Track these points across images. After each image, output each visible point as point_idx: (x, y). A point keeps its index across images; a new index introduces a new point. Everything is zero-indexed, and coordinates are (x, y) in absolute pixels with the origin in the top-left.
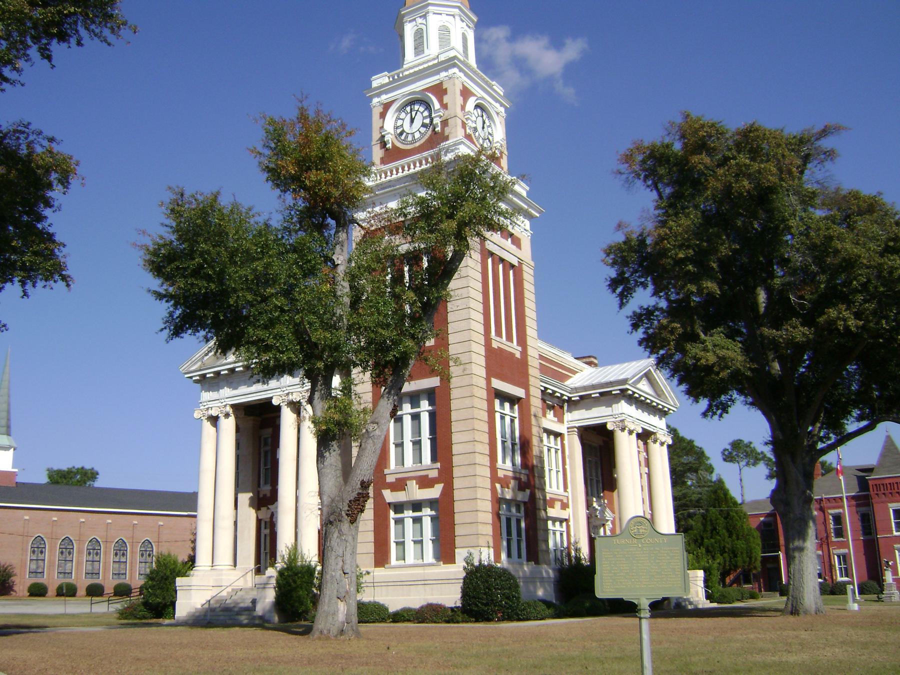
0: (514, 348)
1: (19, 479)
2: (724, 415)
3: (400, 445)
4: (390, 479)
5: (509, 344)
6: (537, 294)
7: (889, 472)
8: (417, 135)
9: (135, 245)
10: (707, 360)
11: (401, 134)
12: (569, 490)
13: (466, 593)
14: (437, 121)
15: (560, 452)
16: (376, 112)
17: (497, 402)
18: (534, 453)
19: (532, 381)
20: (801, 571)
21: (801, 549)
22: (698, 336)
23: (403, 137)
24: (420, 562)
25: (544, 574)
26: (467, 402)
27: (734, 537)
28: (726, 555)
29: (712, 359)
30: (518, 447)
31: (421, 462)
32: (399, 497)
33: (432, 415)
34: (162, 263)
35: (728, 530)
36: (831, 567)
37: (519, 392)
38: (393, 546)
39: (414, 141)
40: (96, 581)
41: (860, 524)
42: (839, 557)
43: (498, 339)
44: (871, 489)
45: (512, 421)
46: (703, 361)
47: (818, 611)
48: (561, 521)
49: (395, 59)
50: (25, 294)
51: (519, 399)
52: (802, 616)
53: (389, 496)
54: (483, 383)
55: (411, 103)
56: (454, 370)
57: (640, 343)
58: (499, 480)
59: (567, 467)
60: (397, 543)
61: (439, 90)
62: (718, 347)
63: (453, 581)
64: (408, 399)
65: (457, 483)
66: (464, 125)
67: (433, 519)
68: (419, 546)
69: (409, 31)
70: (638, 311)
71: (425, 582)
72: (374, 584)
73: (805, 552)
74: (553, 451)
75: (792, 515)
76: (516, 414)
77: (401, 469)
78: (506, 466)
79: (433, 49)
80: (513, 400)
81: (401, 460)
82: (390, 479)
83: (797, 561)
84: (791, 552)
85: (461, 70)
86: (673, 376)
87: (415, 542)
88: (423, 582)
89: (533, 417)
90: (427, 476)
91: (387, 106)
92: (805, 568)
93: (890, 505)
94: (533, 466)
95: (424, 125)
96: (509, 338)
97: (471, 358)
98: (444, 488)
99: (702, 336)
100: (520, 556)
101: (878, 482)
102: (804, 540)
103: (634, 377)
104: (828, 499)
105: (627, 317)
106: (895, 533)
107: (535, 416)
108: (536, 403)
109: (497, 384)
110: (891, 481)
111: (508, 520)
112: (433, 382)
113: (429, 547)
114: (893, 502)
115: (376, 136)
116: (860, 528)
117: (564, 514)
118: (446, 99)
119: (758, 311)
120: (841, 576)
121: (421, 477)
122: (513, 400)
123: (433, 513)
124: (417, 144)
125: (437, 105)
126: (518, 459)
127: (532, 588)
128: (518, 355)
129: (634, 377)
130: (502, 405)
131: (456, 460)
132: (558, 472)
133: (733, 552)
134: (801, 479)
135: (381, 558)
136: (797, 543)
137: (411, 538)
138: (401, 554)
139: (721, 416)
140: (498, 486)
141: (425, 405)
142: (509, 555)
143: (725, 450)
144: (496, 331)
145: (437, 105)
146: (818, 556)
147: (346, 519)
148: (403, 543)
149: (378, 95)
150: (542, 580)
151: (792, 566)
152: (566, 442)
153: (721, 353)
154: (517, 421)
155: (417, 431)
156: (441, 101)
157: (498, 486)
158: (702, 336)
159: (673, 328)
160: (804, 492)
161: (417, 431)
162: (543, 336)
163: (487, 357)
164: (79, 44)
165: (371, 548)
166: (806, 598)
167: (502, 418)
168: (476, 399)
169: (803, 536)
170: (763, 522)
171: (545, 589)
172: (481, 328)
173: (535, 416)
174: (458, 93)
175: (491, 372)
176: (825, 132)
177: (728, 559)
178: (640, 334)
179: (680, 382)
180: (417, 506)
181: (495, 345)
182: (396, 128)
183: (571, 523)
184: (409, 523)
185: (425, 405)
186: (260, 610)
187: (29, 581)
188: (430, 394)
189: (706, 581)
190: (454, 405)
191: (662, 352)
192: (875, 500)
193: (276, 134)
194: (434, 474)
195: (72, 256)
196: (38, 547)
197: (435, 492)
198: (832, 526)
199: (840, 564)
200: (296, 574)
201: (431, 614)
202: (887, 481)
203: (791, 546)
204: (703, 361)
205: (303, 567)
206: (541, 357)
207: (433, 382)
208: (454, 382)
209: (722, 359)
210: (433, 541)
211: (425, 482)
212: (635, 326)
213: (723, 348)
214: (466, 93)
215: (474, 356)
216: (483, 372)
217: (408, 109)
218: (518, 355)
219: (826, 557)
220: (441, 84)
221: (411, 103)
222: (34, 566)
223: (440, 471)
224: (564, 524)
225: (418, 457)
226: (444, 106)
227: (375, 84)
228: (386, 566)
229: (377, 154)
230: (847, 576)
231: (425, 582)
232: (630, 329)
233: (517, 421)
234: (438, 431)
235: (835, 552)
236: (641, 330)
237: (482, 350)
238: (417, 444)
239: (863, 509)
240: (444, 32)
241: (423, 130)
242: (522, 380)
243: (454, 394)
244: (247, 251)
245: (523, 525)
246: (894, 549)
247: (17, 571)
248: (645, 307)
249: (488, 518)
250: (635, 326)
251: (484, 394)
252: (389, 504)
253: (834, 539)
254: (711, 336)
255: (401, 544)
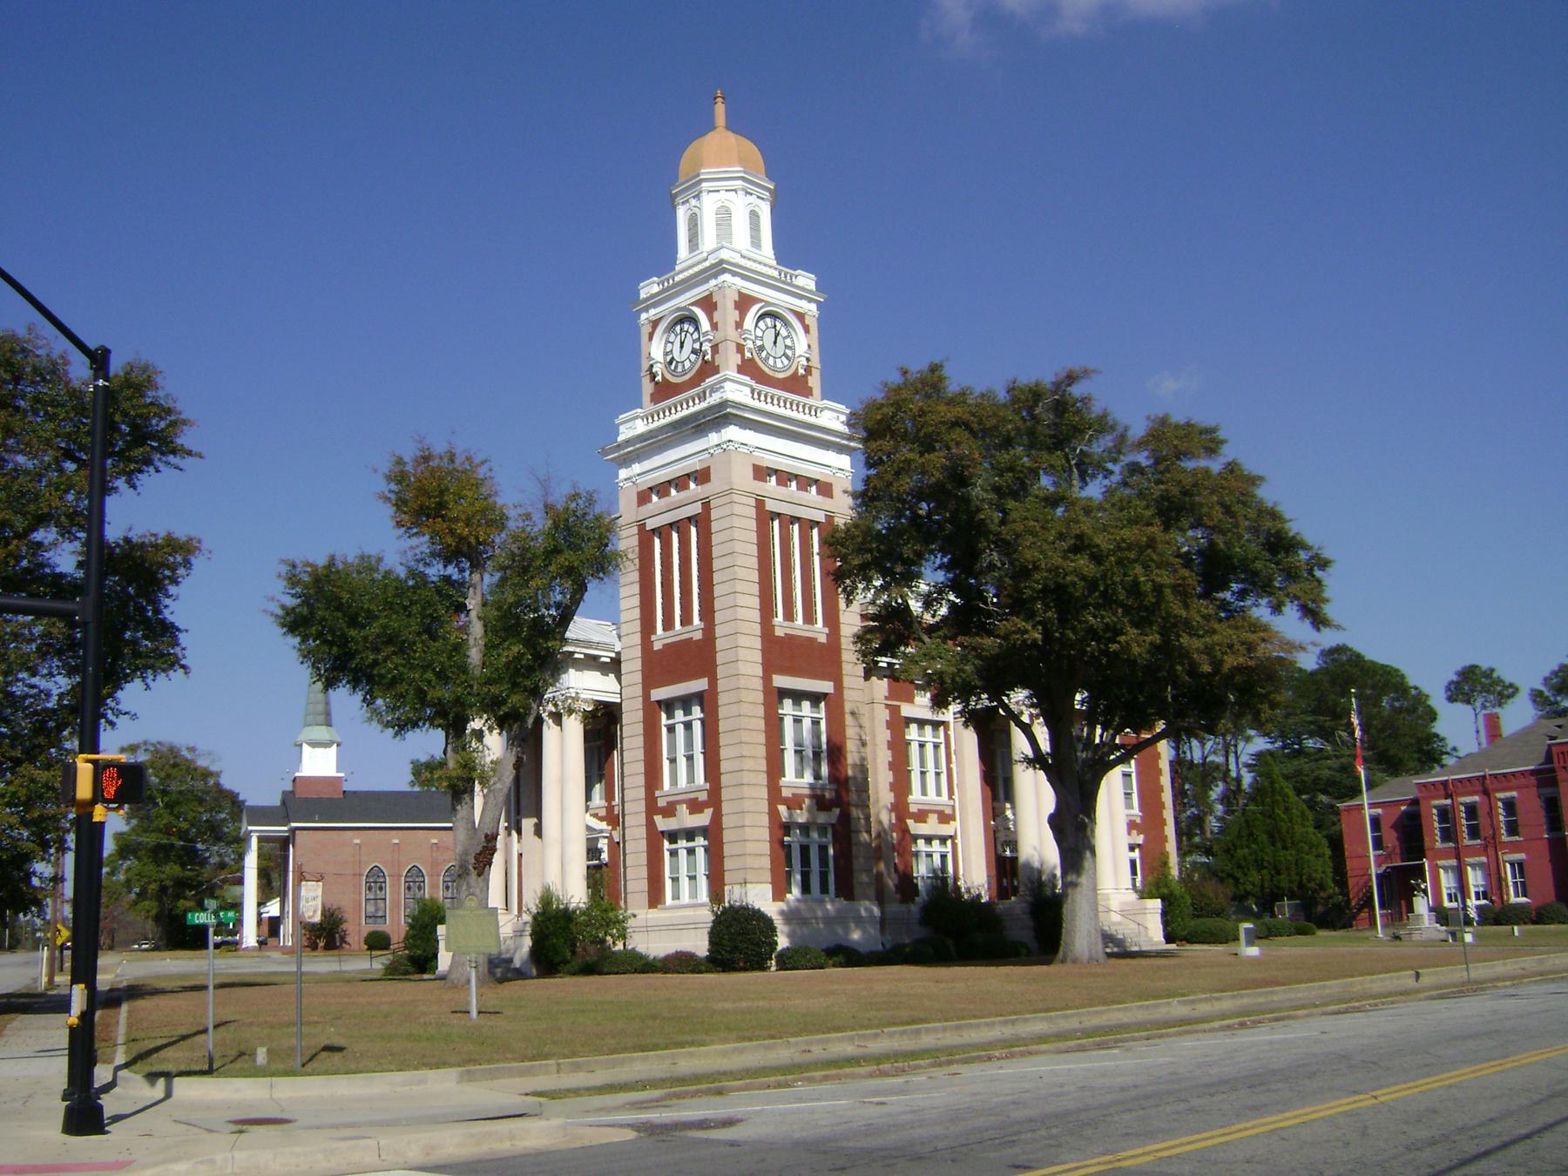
1: (347, 787)
8: (687, 364)
9: (265, 611)
11: (670, 363)
12: (956, 797)
13: (715, 936)
14: (707, 347)
15: (943, 747)
16: (646, 330)
18: (850, 761)
25: (863, 913)
27: (1279, 845)
28: (1265, 872)
30: (824, 755)
34: (295, 623)
35: (1271, 836)
36: (1500, 881)
37: (826, 686)
39: (685, 372)
40: (380, 928)
41: (1543, 813)
42: (1512, 865)
48: (943, 840)
49: (664, 260)
50: (148, 687)
51: (824, 696)
53: (662, 823)
55: (681, 321)
56: (720, 672)
58: (786, 801)
59: (953, 766)
61: (708, 304)
66: (740, 349)
69: (682, 214)
74: (929, 748)
76: (823, 714)
78: (796, 779)
79: (708, 240)
80: (815, 698)
81: (674, 781)
85: (734, 274)
91: (655, 324)
94: (847, 779)
95: (694, 352)
100: (824, 889)
104: (1495, 776)
111: (805, 850)
112: (700, 685)
115: (645, 366)
116: (1544, 820)
117: (946, 830)
118: (717, 316)
120: (1517, 895)
122: (815, 698)
124: (687, 377)
125: (705, 325)
126: (825, 770)
127: (840, 931)
131: (724, 779)
132: (938, 774)
133: (1275, 867)
140: (782, 809)
141: (697, 712)
142: (806, 888)
143: (1452, 682)
145: (705, 325)
147: (474, 873)
149: (646, 310)
150: (859, 921)
152: (951, 732)
155: (689, 744)
156: (711, 319)
157: (782, 809)
161: (689, 744)
163: (766, 651)
164: (158, 471)
165: (644, 885)
170: (1405, 812)
171: (864, 931)
173: (853, 713)
174: (730, 305)
176: (1071, 378)
177: (1267, 877)
180: (690, 834)
181: (779, 632)
182: (666, 354)
183: (958, 841)
184: (683, 854)
185: (697, 712)
186: (517, 963)
187: (366, 928)
189: (1164, 914)
193: (399, 477)
194: (703, 796)
195: (191, 645)
196: (376, 880)
197: (703, 819)
198: (1502, 818)
199: (1514, 877)
201: (681, 963)
207: (700, 685)
211: (695, 807)
214: (744, 302)
217: (678, 328)
219: (1493, 866)
221: (681, 321)
222: (371, 909)
224: (949, 842)
226: (714, 326)
227: (643, 295)
229: (647, 388)
230: (1525, 895)
235: (1507, 857)
238: (690, 758)
239: (1548, 791)
240: (724, 216)
241: (693, 357)
244: (369, 611)
245: (831, 851)
247: (348, 916)
249: (765, 848)
253: (1505, 838)
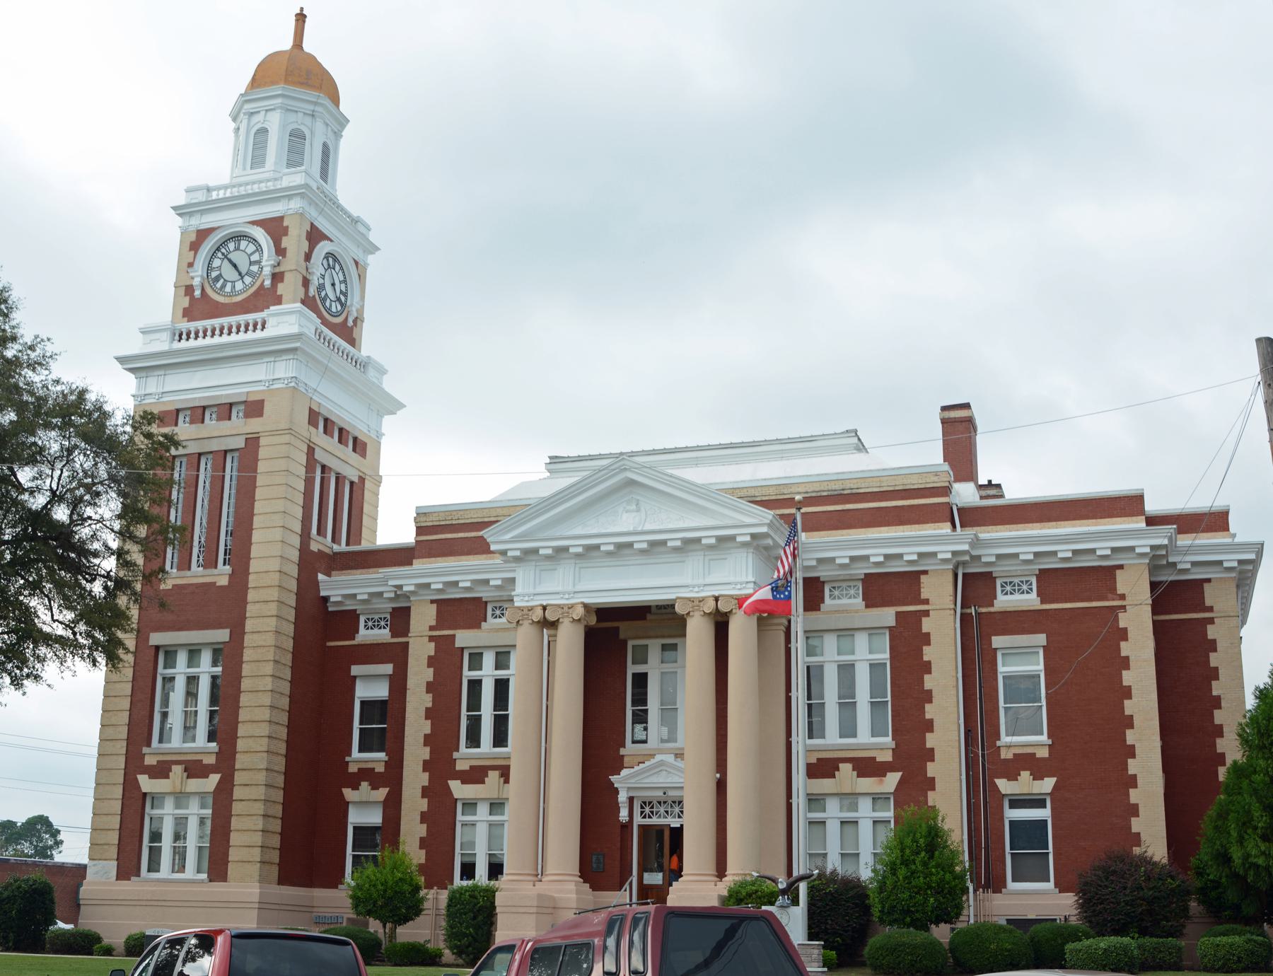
11: (217, 279)
23: (219, 285)
43: (320, 539)
65: (239, 778)
66: (306, 283)
82: (150, 761)
124: (239, 298)
191: (942, 933)
194: (210, 760)
207: (222, 635)
220: (282, 218)
225: (189, 729)
226: (281, 251)
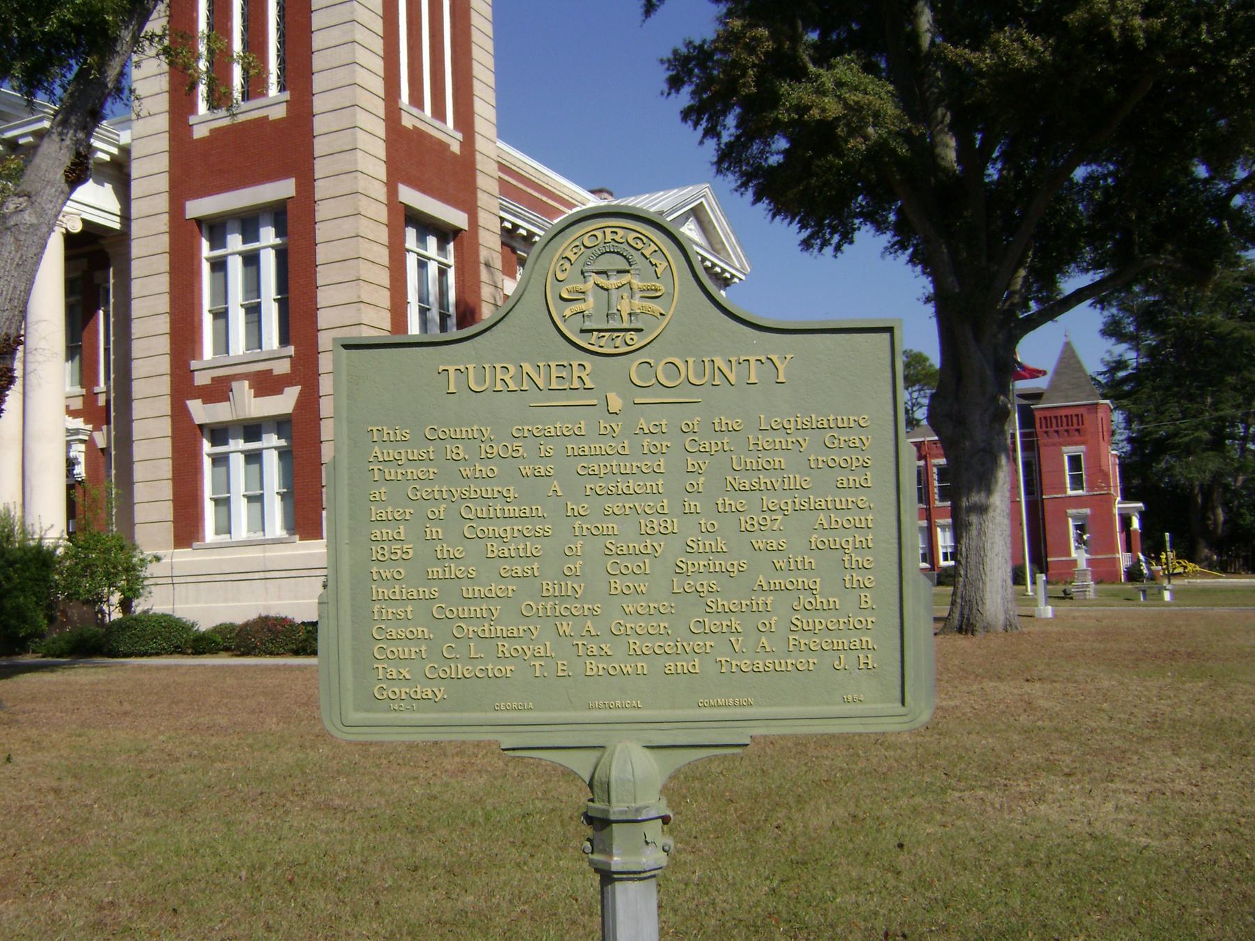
0: (448, 132)
2: (845, 247)
3: (221, 315)
4: (201, 379)
5: (437, 124)
6: (499, 55)
7: (1066, 398)
10: (823, 110)
17: (411, 234)
19: (482, 199)
20: (981, 551)
21: (982, 509)
22: (805, 68)
24: (258, 536)
26: (347, 226)
29: (833, 108)
31: (260, 347)
32: (219, 413)
33: (282, 255)
37: (457, 218)
38: (209, 509)
43: (415, 111)
44: (1038, 425)
45: (442, 273)
46: (815, 112)
47: (1008, 626)
52: (980, 635)
53: (200, 412)
54: (381, 192)
57: (686, 115)
60: (217, 501)
62: (845, 90)
63: (256, 576)
64: (237, 225)
67: (283, 454)
68: (258, 505)
70: (684, 51)
71: (266, 574)
72: (172, 580)
73: (991, 514)
75: (967, 444)
76: (451, 260)
77: (222, 359)
80: (446, 234)
81: (223, 343)
82: (201, 379)
83: (974, 533)
84: (963, 515)
86: (744, 185)
87: (250, 499)
88: (262, 575)
89: (482, 268)
90: (271, 371)
92: (988, 546)
93: (1065, 449)
96: (439, 112)
97: (355, 140)
98: (301, 394)
99: (812, 68)
101: (1048, 414)
102: (989, 492)
103: (673, 211)
105: (662, 62)
106: (1070, 492)
107: (487, 265)
108: (490, 244)
109: (410, 196)
110: (1068, 412)
112: (284, 189)
113: (275, 509)
114: (1069, 444)
119: (918, 47)
121: (259, 374)
122: (446, 234)
123: (283, 443)
128: (456, 148)
129: (673, 211)
130: (421, 239)
134: (989, 372)
135: (186, 529)
136: (975, 498)
137: (242, 492)
138: (224, 523)
139: (838, 248)
141: (268, 236)
144: (411, 96)
146: (921, 528)
148: (227, 501)
151: (963, 541)
153: (852, 97)
154: (451, 274)
155: (253, 286)
158: (812, 68)
159: (753, 38)
160: (994, 399)
161: (253, 286)
162: (505, 131)
165: (167, 511)
166: (988, 602)
167: (422, 265)
168: (364, 221)
169: (985, 482)
172: (378, 86)
173: (487, 265)
175: (397, 173)
178: (684, 97)
179: (757, 199)
180: (252, 430)
181: (407, 122)
184: (237, 462)
185: (268, 236)
188: (278, 213)
190: (322, 232)
192: (1043, 440)
197: (284, 403)
200: (11, 564)
202: (1063, 412)
203: (964, 503)
204: (815, 112)
205: (24, 549)
206: (503, 167)
207: (284, 189)
208: (321, 189)
209: (857, 109)
210: (283, 496)
211: (266, 384)
212: (675, 83)
213: (856, 89)
215: (361, 136)
216: (381, 171)
218: (456, 148)
223: (294, 361)
228: (196, 544)
231: (266, 574)
232: (665, 87)
233: (451, 274)
234: (291, 283)
236: (687, 90)
237: (380, 129)
238: (253, 311)
242: (466, 199)
243: (322, 211)
246: (1067, 516)
248: (697, 43)
250: (675, 83)
251: (382, 214)
252: (201, 426)
254: (830, 67)
255: (223, 503)
